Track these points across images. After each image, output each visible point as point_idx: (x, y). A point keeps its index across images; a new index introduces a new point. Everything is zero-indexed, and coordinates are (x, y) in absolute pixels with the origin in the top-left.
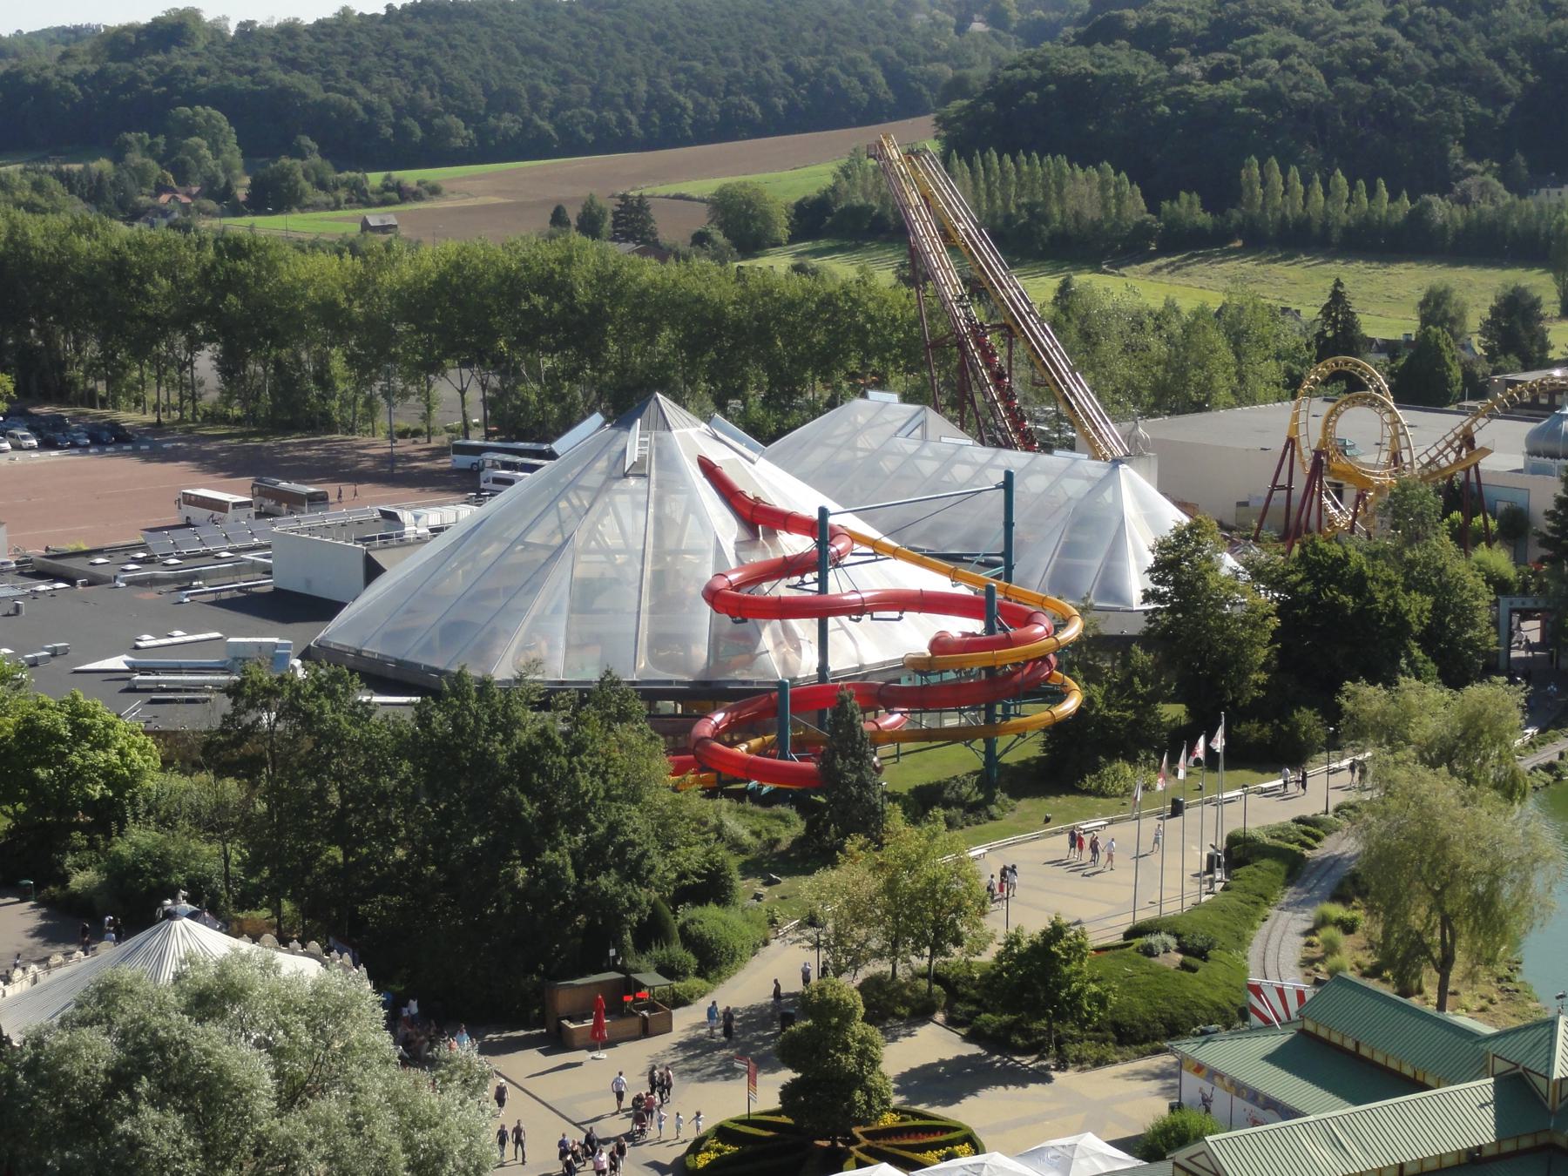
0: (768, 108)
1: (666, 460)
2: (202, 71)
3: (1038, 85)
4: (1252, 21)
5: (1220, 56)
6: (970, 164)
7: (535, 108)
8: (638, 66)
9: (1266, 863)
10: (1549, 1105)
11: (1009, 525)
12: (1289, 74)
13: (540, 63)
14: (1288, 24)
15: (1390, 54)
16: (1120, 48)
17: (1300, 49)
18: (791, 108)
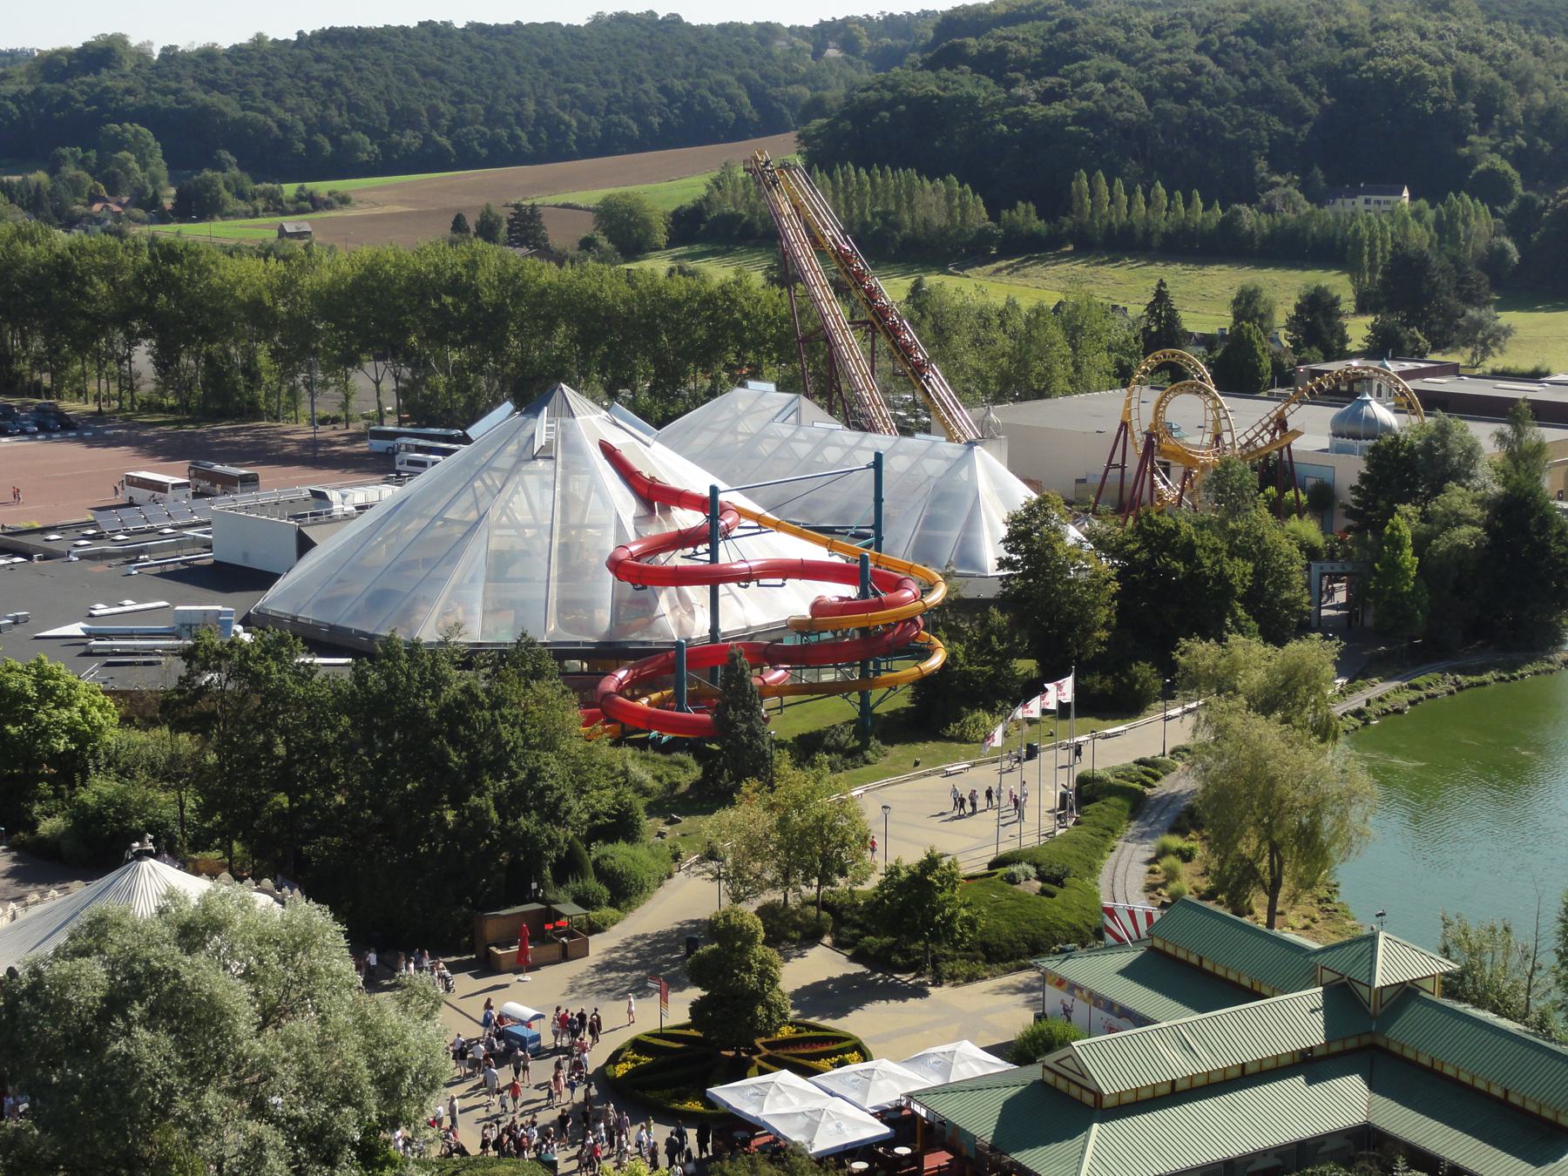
0: (645, 127)
1: (573, 448)
2: (129, 91)
3: (890, 106)
4: (1079, 48)
5: (1052, 80)
6: (831, 177)
7: (434, 125)
8: (527, 88)
9: (1113, 800)
10: (1371, 1010)
11: (878, 500)
12: (1114, 96)
13: (438, 84)
14: (1112, 52)
15: (1203, 78)
16: (962, 73)
17: (1123, 74)
18: (666, 125)
